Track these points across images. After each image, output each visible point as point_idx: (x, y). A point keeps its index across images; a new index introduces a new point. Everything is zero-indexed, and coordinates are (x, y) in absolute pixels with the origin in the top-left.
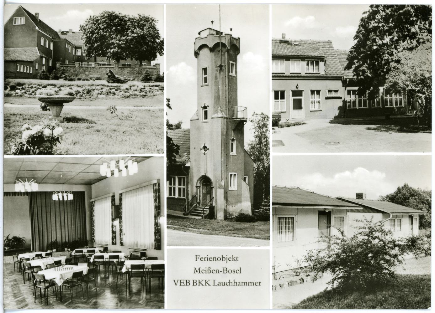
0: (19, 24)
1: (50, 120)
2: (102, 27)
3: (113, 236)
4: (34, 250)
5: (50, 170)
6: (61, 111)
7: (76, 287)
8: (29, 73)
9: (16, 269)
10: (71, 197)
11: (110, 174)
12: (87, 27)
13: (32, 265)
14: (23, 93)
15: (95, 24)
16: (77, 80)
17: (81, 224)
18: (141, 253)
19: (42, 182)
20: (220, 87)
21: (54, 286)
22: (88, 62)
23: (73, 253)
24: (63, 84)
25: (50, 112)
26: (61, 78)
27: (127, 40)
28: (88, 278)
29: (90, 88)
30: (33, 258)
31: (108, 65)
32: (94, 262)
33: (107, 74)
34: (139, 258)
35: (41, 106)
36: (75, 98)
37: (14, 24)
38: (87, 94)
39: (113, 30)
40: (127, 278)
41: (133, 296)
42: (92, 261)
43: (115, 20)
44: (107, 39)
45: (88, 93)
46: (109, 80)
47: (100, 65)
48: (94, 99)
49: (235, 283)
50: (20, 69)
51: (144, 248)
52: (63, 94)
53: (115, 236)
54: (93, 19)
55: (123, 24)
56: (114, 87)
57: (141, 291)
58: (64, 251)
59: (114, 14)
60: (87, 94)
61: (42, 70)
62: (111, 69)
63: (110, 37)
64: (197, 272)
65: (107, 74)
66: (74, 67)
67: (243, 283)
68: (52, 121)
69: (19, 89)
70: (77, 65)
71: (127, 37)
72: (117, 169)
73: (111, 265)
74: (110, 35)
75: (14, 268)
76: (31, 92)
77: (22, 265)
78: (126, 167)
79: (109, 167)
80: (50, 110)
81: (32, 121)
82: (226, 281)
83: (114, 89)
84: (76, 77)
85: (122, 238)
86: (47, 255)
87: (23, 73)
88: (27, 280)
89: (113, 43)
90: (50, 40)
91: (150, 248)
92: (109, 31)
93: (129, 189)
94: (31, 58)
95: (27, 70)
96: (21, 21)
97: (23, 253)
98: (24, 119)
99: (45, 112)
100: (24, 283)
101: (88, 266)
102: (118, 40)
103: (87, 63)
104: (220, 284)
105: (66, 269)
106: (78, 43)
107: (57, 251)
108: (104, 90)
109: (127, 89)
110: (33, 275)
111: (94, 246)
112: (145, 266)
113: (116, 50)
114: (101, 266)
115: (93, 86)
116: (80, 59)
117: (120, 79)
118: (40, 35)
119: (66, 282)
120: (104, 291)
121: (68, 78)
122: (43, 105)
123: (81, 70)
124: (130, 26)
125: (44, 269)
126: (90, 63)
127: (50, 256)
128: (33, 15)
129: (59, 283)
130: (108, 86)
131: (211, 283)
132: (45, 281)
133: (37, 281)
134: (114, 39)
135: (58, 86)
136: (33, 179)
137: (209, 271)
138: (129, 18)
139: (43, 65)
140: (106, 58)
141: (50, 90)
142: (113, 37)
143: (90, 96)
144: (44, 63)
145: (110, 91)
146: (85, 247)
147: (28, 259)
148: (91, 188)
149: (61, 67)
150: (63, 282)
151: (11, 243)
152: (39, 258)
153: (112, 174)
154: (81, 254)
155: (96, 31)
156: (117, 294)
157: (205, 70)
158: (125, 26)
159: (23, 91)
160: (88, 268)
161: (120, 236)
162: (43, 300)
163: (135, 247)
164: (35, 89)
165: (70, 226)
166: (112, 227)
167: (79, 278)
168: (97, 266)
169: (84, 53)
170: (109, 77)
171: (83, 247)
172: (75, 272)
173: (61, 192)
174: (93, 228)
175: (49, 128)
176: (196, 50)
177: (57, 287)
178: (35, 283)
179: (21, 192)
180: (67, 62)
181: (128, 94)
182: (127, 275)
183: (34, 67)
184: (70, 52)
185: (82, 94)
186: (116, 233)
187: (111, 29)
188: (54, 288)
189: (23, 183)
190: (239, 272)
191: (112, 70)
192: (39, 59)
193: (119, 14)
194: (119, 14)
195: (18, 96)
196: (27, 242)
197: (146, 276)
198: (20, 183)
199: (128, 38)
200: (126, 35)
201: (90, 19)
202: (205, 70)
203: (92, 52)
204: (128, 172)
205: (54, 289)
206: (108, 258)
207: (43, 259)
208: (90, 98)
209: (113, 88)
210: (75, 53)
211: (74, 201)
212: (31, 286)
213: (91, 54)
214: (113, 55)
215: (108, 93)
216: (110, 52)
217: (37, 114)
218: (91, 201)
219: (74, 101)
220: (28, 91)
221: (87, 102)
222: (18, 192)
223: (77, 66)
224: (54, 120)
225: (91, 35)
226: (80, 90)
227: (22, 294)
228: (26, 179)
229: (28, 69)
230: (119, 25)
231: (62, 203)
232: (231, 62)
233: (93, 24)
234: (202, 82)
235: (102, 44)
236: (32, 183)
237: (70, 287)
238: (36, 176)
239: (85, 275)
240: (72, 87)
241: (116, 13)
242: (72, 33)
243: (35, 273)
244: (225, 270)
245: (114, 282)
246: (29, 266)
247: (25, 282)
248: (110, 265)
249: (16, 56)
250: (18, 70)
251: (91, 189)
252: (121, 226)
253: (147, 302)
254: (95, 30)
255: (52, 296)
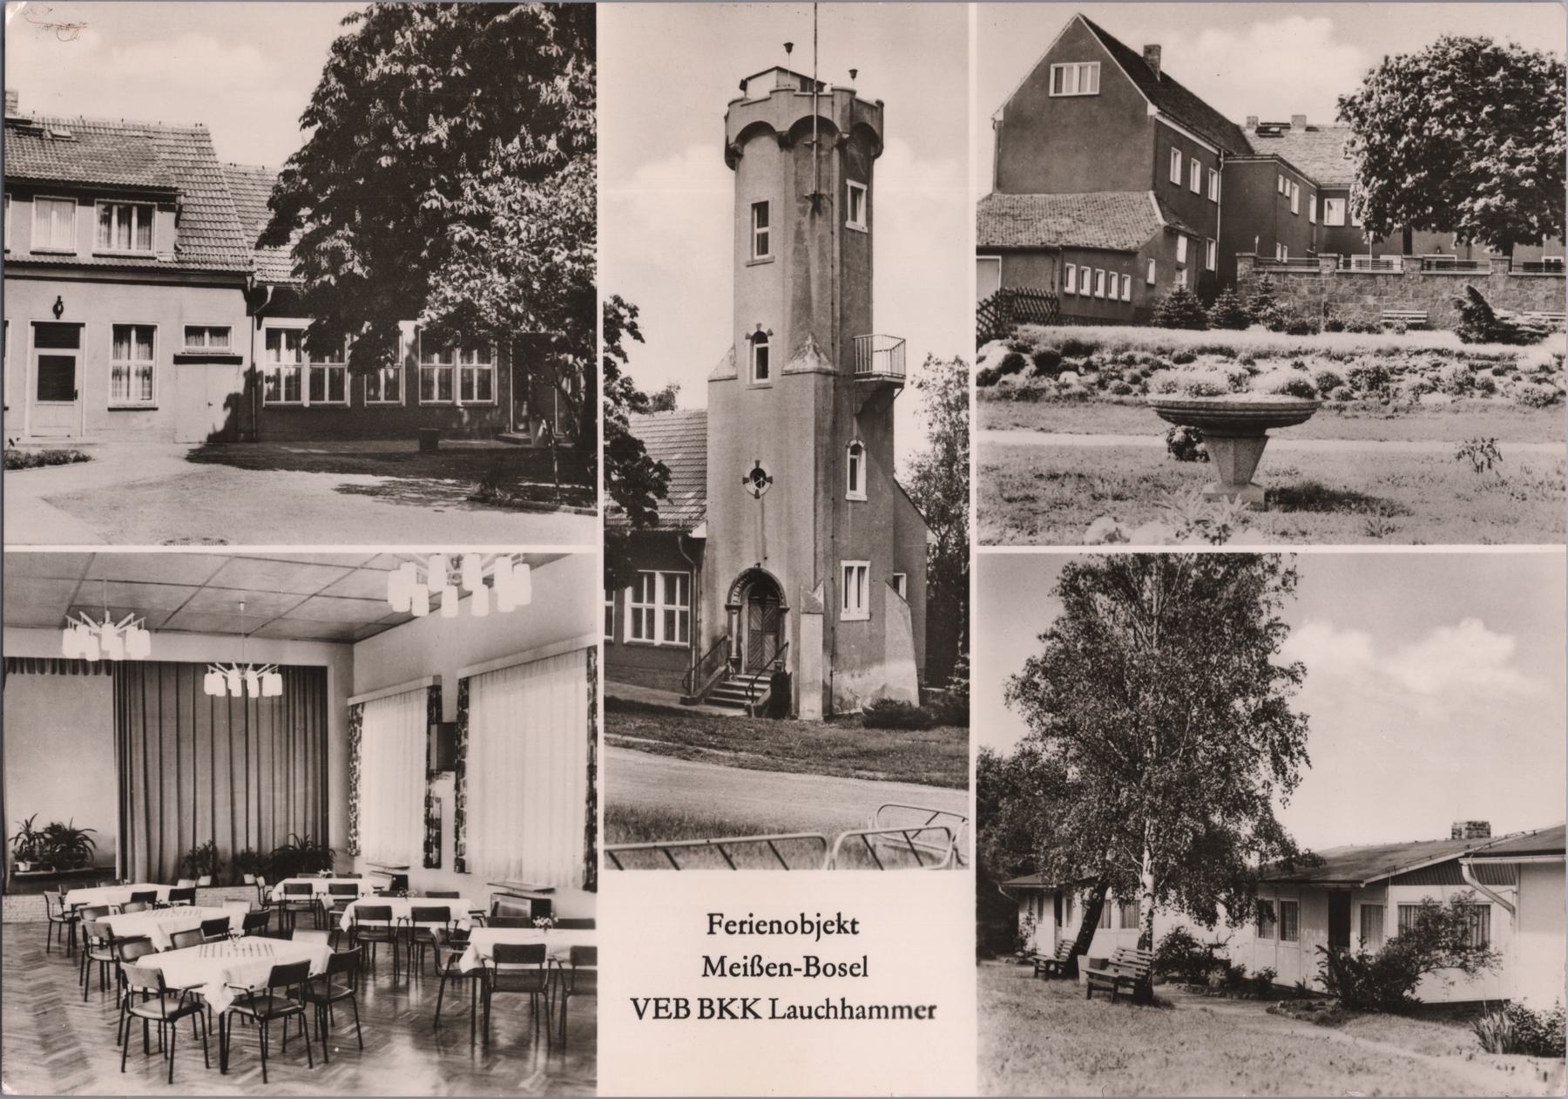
0: (1075, 92)
1: (1209, 500)
2: (1438, 105)
3: (429, 836)
4: (126, 876)
5: (200, 582)
6: (1257, 461)
7: (282, 1020)
8: (1119, 302)
9: (54, 944)
10: (274, 685)
11: (426, 608)
12: (1373, 104)
13: (117, 932)
14: (1090, 386)
15: (1405, 92)
16: (1327, 329)
17: (310, 788)
18: (535, 902)
19: (168, 625)
20: (815, 271)
21: (198, 1014)
22: (1376, 255)
23: (277, 893)
24: (1265, 347)
25: (1209, 464)
26: (1256, 321)
27: (1544, 158)
28: (329, 988)
29: (1384, 363)
30: (124, 905)
31: (1461, 265)
32: (354, 930)
33: (1460, 304)
34: (526, 923)
35: (1169, 441)
36: (1319, 405)
37: (1052, 93)
38: (1371, 388)
39: (1483, 115)
40: (478, 993)
41: (498, 1060)
42: (345, 924)
43: (1493, 74)
44: (1460, 154)
45: (1373, 385)
46: (1466, 329)
47: (1429, 265)
48: (1403, 409)
49: (846, 1011)
50: (1080, 284)
51: (544, 886)
52: (1264, 389)
53: (439, 836)
54: (1398, 71)
55: (1526, 92)
56: (1489, 358)
57: (529, 1042)
58: (243, 884)
59: (1488, 50)
60: (1371, 388)
61: (1172, 286)
62: (1474, 281)
63: (1471, 147)
64: (714, 972)
65: (1460, 304)
66: (1315, 274)
67: (875, 1011)
68: (1218, 505)
69: (1075, 368)
70: (1327, 265)
71: (1543, 148)
72: (455, 589)
73: (418, 943)
74: (1471, 138)
75: (49, 940)
76: (1127, 379)
77: (79, 931)
78: (488, 581)
79: (422, 580)
80: (1207, 459)
81: (1129, 503)
82: (817, 1001)
83: (1489, 366)
84: (1322, 317)
85: (463, 846)
86: (175, 895)
87: (1106, 304)
88: (95, 989)
89: (1484, 174)
90: (1211, 163)
91: (566, 886)
92: (1468, 120)
93: (498, 664)
94: (1127, 237)
95: (1108, 289)
96: (1081, 79)
97: (82, 887)
98: (1097, 498)
99: (1187, 467)
100: (82, 998)
101: (330, 943)
102: (1507, 160)
103: (1370, 258)
104: (793, 1013)
105: (247, 952)
106: (1331, 172)
107: (215, 884)
108: (1445, 373)
109: (1544, 368)
110: (118, 968)
111: (357, 871)
112: (548, 951)
113: (1496, 201)
114: (378, 944)
115: (1396, 357)
116: (1340, 242)
117: (1514, 327)
118: (1165, 142)
119: (246, 999)
120: (387, 1039)
121: (1287, 320)
122: (1179, 435)
123: (1345, 287)
124: (1557, 101)
125: (161, 948)
126: (1383, 258)
127: (188, 901)
128: (1134, 54)
129: (219, 1001)
130: (1461, 356)
131: (763, 1008)
132: (164, 992)
133: (134, 993)
134: (1490, 154)
135: (1242, 355)
136: (132, 616)
137: (756, 967)
138: (1554, 66)
139: (1179, 268)
140: (1455, 235)
141: (1210, 373)
142: (1483, 146)
143: (1385, 399)
144: (1181, 256)
145: (1473, 375)
146: (322, 872)
147: (103, 911)
148: (351, 654)
149: (1258, 273)
150: (232, 999)
151: (41, 847)
152: (144, 909)
153: (435, 606)
154: (306, 897)
155: (1411, 122)
156: (439, 1050)
157: (761, 210)
158: (1534, 99)
159: (1092, 377)
160: (331, 951)
161: (457, 837)
162: (151, 1065)
163: (513, 881)
164: (1144, 367)
165: (266, 794)
166: (429, 802)
167: (292, 987)
168: (365, 944)
169: (1358, 215)
170: (1468, 315)
171: (312, 870)
172: (280, 963)
173: (239, 666)
174: (355, 805)
175: (1206, 536)
176: (732, 140)
177: (210, 1017)
178: (126, 1001)
179: (84, 661)
180: (1281, 254)
181: (1547, 389)
182: (479, 981)
183: (1138, 274)
184: (1295, 209)
185: (1347, 388)
186: (422, 818)
187: (1476, 111)
188: (198, 1019)
189: (94, 628)
190: (861, 971)
191: (1480, 287)
192: (1160, 240)
193: (1512, 47)
194: (1512, 47)
195: (1069, 396)
196: (100, 845)
197: (551, 986)
198: (81, 628)
199: (1549, 150)
200: (1538, 140)
201: (1383, 71)
202: (761, 210)
203: (1394, 209)
204: (493, 600)
205: (199, 1025)
206: (409, 915)
207: (160, 911)
208: (1383, 407)
209: (1485, 362)
210: (1320, 214)
211: (284, 703)
212: (110, 1010)
213: (1389, 220)
214: (1482, 224)
215: (1463, 386)
216: (1471, 210)
217: (1155, 473)
218: (351, 702)
219: (1315, 420)
220: (1112, 378)
221: (1376, 424)
222: (75, 661)
223: (1326, 271)
224: (1226, 498)
225: (1388, 137)
226: (1341, 370)
227: (72, 1037)
228: (108, 614)
229: (1115, 281)
230: (1508, 96)
231: (242, 708)
232: (850, 183)
233: (1397, 94)
234: (749, 253)
235: (1437, 175)
236: (129, 628)
237: (258, 1018)
238: (144, 604)
239: (319, 977)
240: (1307, 360)
241: (1495, 45)
242: (1302, 131)
243: (128, 961)
244: (813, 966)
245: (428, 1006)
246: (105, 936)
247: (86, 995)
248: (414, 942)
249: (1059, 228)
250: (1071, 289)
251: (352, 660)
252: (460, 799)
253: (550, 1086)
254: (1407, 116)
255: (188, 1048)
